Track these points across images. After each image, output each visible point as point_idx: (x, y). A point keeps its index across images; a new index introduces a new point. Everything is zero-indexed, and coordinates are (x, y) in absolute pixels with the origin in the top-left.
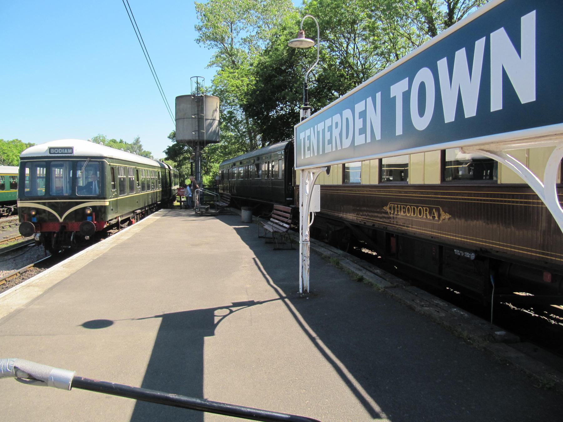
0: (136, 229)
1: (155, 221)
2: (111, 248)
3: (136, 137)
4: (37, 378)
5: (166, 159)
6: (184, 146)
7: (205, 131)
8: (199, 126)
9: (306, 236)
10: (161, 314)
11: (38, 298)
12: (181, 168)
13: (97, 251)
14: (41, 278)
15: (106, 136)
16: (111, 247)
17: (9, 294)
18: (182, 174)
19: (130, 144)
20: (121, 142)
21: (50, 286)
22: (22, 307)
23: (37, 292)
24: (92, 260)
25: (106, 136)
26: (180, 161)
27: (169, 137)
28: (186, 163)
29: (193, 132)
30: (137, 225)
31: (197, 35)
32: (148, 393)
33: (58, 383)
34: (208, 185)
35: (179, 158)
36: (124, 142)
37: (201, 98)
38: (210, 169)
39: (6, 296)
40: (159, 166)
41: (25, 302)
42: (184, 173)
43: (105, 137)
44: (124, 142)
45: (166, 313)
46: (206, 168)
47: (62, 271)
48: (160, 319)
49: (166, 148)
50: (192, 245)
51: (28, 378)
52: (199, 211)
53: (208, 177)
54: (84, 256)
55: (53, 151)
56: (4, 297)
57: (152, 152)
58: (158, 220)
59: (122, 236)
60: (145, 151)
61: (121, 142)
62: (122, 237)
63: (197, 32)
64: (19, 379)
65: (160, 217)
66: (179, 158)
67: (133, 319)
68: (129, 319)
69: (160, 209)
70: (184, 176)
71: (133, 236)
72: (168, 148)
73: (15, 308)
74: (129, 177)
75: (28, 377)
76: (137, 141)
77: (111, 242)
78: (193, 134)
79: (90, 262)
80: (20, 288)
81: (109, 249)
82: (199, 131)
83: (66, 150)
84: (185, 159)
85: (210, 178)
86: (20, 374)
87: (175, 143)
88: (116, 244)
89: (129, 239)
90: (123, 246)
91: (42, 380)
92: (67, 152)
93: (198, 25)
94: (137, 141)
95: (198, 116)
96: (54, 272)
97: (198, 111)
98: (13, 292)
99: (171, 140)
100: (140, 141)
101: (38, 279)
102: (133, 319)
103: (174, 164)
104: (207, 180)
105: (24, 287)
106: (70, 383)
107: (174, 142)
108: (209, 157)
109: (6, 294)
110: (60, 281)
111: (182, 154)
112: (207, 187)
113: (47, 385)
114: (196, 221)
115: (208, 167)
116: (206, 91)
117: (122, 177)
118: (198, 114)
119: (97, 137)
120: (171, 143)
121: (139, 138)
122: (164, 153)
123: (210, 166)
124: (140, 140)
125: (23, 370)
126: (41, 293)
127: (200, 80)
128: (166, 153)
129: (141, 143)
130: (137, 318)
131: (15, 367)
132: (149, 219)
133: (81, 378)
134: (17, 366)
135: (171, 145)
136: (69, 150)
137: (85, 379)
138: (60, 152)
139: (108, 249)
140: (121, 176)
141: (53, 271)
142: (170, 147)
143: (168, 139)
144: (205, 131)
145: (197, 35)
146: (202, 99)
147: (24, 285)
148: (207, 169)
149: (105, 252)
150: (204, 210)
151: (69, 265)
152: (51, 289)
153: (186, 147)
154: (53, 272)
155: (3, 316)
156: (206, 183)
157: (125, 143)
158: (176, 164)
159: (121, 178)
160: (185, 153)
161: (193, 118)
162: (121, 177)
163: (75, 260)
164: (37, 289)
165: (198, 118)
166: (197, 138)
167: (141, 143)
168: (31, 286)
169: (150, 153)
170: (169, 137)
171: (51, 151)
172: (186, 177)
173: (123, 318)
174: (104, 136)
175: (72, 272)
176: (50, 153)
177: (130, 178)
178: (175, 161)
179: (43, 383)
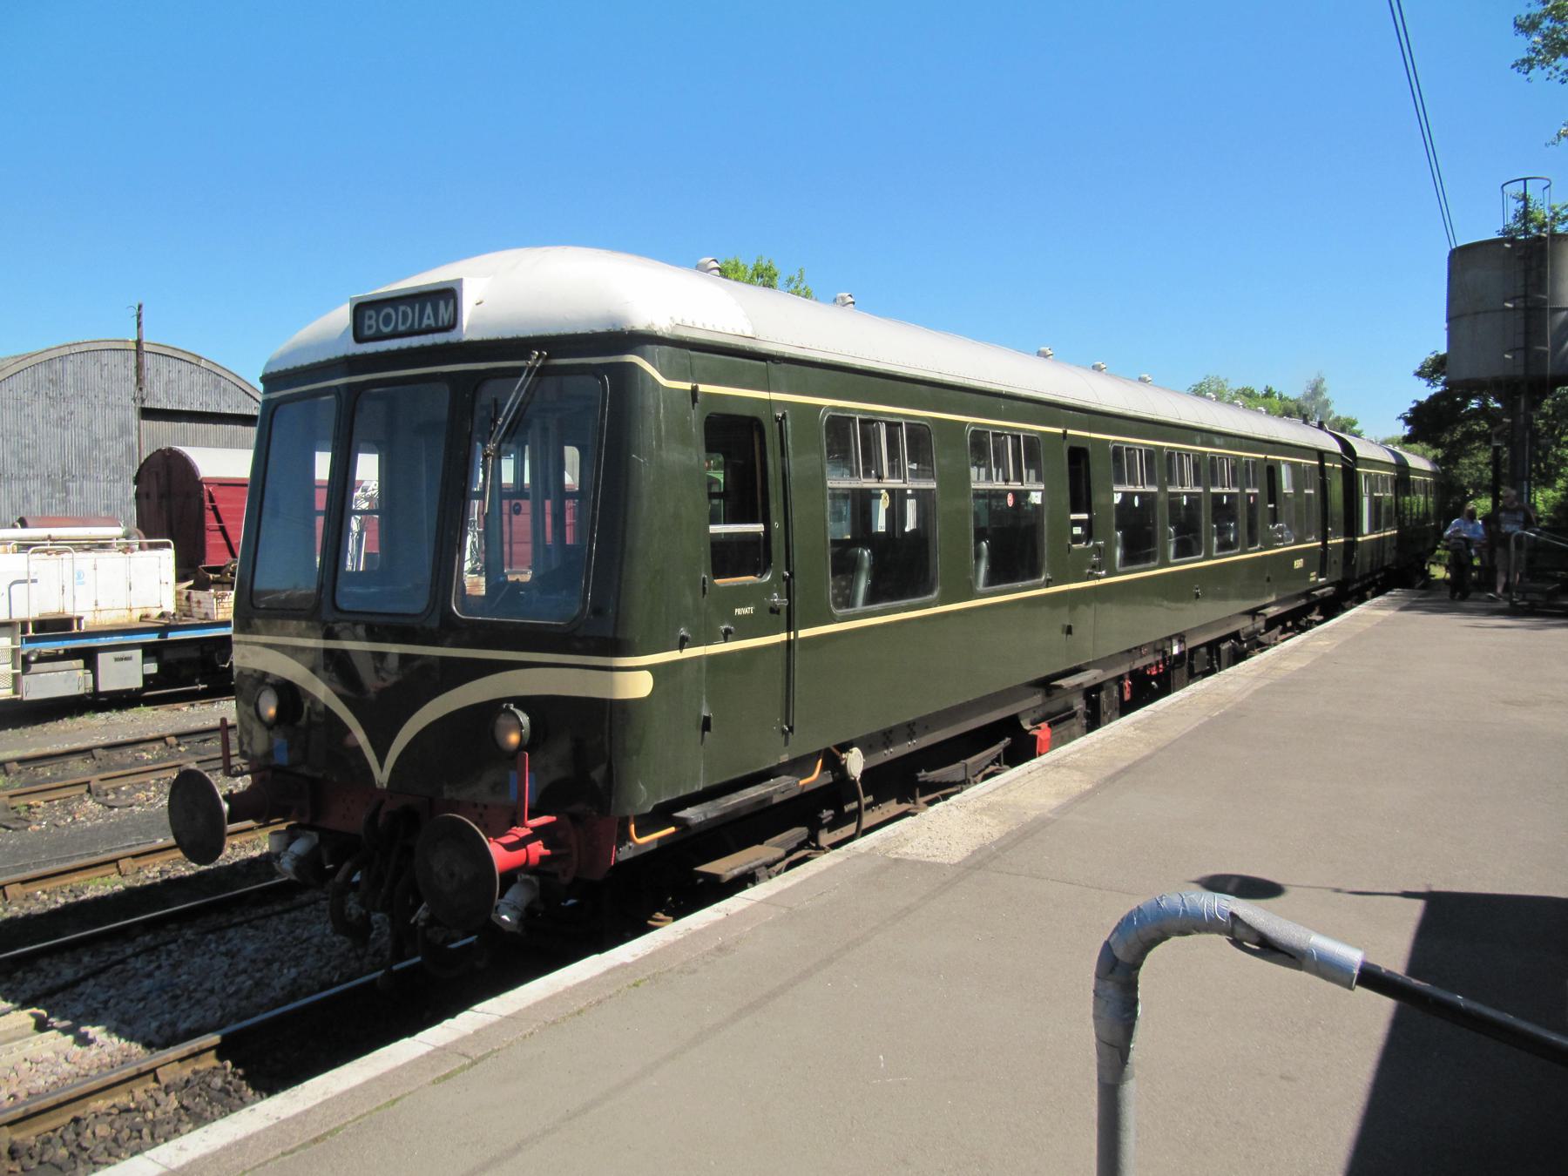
0: (1321, 643)
1: (1378, 624)
2: (1257, 692)
3: (1313, 377)
4: (1280, 948)
5: (1408, 440)
6: (1467, 398)
7: (1548, 349)
8: (1527, 333)
9: (97, 889)
10: (1422, 889)
11: (1083, 797)
12: (1456, 463)
13: (1218, 694)
14: (1084, 749)
15: (1226, 380)
16: (1256, 688)
17: (1017, 778)
18: (1456, 485)
19: (1294, 400)
20: (1269, 394)
21: (1109, 772)
22: (1050, 815)
23: (1077, 783)
24: (1206, 719)
25: (1226, 380)
26: (1453, 444)
27: (1419, 374)
28: (1474, 449)
29: (1508, 352)
30: (1325, 631)
31: (1522, 46)
32: (1554, 1041)
33: (1328, 969)
34: (1549, 519)
35: (1451, 435)
36: (1277, 395)
37: (1539, 244)
38: (1557, 468)
39: (1009, 782)
40: (1393, 460)
41: (1054, 803)
42: (1465, 481)
43: (1225, 384)
44: (1277, 395)
45: (1435, 889)
46: (1542, 465)
47: (1132, 739)
48: (1418, 906)
49: (1406, 406)
50: (1505, 702)
51: (1257, 945)
52: (1523, 600)
53: (1549, 493)
54: (1183, 705)
55: (373, 322)
56: (1005, 785)
57: (1358, 420)
58: (1385, 621)
59: (1281, 659)
60: (1338, 419)
61: (1269, 394)
62: (1284, 664)
63: (1522, 37)
64: (1237, 943)
65: (1392, 612)
66: (1451, 435)
67: (1338, 891)
68: (1327, 888)
69: (1391, 590)
70: (1463, 490)
71: (1314, 661)
72: (1414, 405)
73: (1033, 813)
74: (1213, 490)
75: (1257, 940)
76: (1316, 391)
77: (1254, 673)
78: (1505, 358)
79: (1201, 722)
80: (1039, 768)
81: (1250, 691)
82: (1527, 349)
83: (429, 310)
84: (1470, 436)
85: (1558, 494)
86: (1240, 931)
87: (1439, 389)
88: (1268, 682)
89: (1301, 669)
90: (1288, 686)
91: (1292, 954)
92: (432, 322)
93: (1524, 16)
94: (1316, 391)
95: (1526, 302)
96: (1113, 738)
97: (1526, 286)
98: (1024, 776)
99: (1424, 382)
100: (1325, 390)
101: (1078, 751)
102: (1338, 891)
103: (1431, 454)
104: (1545, 501)
105: (1047, 768)
106: (1356, 972)
107: (1435, 386)
108: (1553, 428)
109: (1009, 779)
110: (1131, 762)
111: (1462, 420)
112: (1544, 523)
113: (1300, 967)
114: (1513, 630)
115: (1551, 460)
116: (1553, 219)
117: (1226, 490)
118: (1526, 296)
119: (1201, 385)
120: (1424, 391)
121: (1322, 380)
122: (1402, 422)
123: (1556, 456)
124: (1325, 385)
125: (1248, 922)
126: (1089, 787)
127: (1534, 191)
128: (1408, 421)
129: (1326, 396)
130: (1351, 890)
131: (1232, 915)
132: (1356, 616)
133: (1380, 968)
134: (1236, 912)
135: (1424, 398)
136: (442, 304)
137: (1388, 972)
138: (401, 328)
139: (1247, 693)
140: (1182, 485)
141: (1110, 736)
142: (1420, 404)
143: (1416, 377)
144: (1548, 349)
145: (1522, 46)
146: (1543, 250)
147: (1046, 762)
148: (1548, 466)
149: (1239, 699)
150: (1537, 597)
151: (1149, 723)
152: (1113, 779)
153: (1473, 401)
154: (1111, 739)
155: (1009, 830)
156: (1543, 512)
157: (1281, 398)
158: (1439, 453)
159: (1221, 495)
160: (1470, 418)
161: (1508, 309)
162: (1179, 489)
163: (1161, 714)
164: (1077, 776)
165: (1527, 309)
166: (1520, 371)
167: (1326, 396)
168: (1064, 766)
169: (1353, 423)
170: (1419, 374)
171: (367, 322)
172: (1471, 492)
173: (1308, 883)
174: (1222, 379)
175: (1160, 744)
176: (359, 338)
177: (1218, 496)
178: (1436, 445)
179: (1293, 960)
